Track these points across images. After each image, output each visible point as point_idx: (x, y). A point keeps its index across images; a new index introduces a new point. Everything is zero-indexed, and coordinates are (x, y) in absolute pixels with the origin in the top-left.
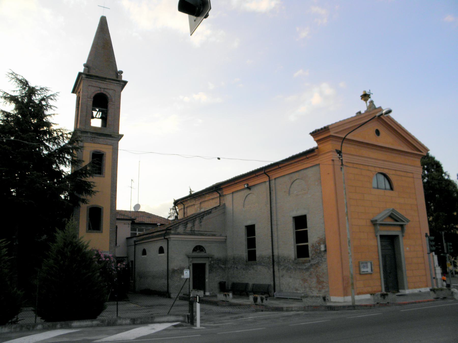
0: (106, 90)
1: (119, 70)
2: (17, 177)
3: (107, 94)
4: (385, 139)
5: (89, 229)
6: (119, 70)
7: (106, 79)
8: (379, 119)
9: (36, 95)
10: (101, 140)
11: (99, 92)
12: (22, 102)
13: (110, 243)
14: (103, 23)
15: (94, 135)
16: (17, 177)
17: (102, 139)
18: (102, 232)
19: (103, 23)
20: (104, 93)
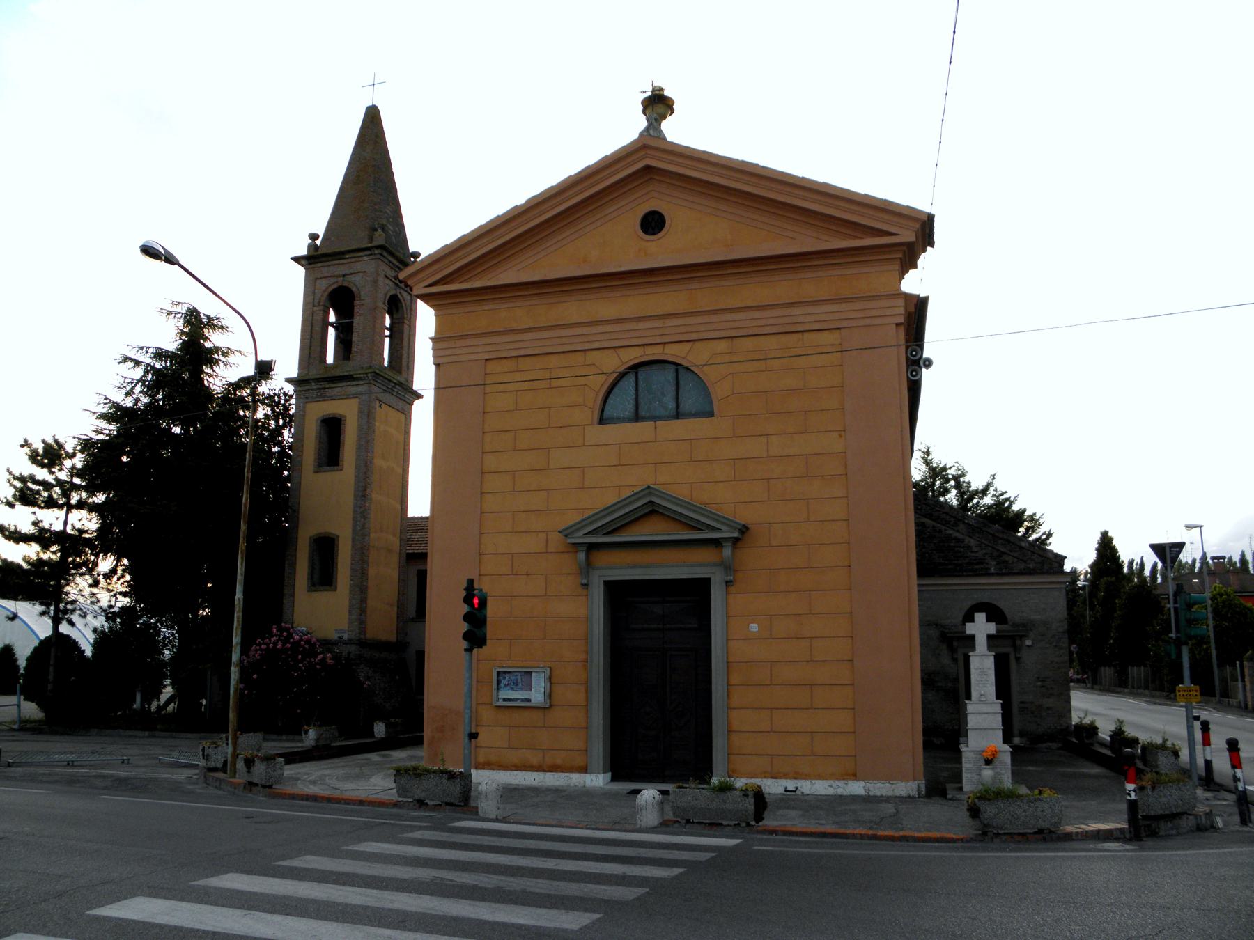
0: (347, 278)
1: (411, 250)
2: (195, 428)
3: (351, 286)
4: (694, 234)
5: (313, 585)
6: (411, 250)
7: (343, 253)
8: (931, 218)
9: (75, 618)
10: (336, 390)
11: (335, 286)
12: (60, 550)
13: (350, 612)
14: (372, 119)
15: (323, 384)
16: (195, 428)
17: (338, 389)
18: (335, 589)
19: (372, 119)
20: (345, 284)
